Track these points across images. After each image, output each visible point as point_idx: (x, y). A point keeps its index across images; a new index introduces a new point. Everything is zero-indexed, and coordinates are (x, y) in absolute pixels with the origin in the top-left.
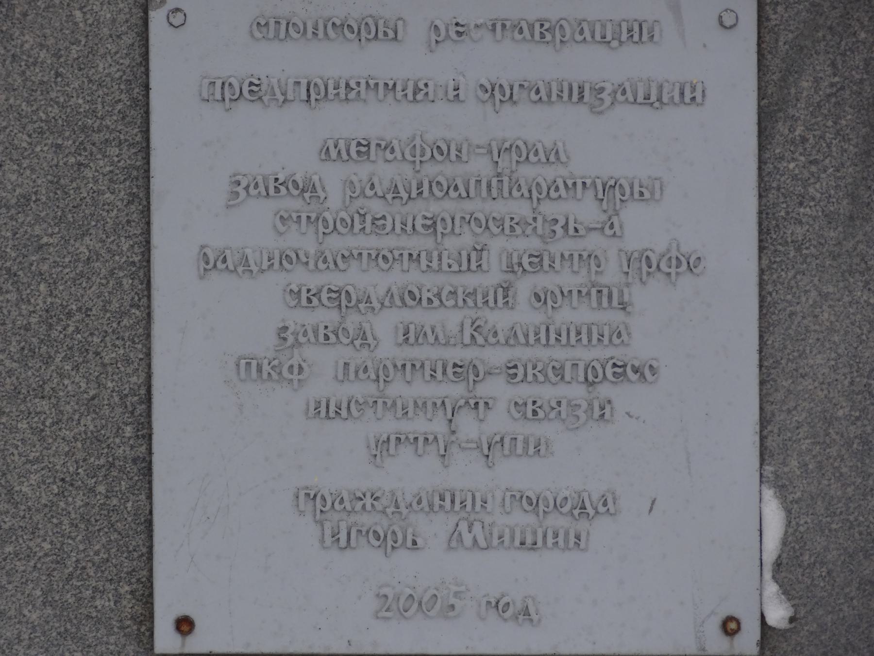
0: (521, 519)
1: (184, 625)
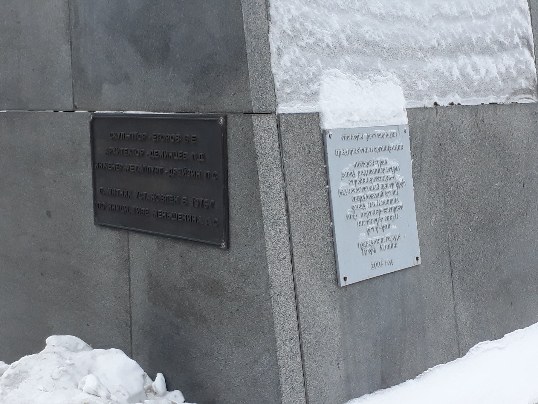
0: (389, 243)
1: (345, 279)
